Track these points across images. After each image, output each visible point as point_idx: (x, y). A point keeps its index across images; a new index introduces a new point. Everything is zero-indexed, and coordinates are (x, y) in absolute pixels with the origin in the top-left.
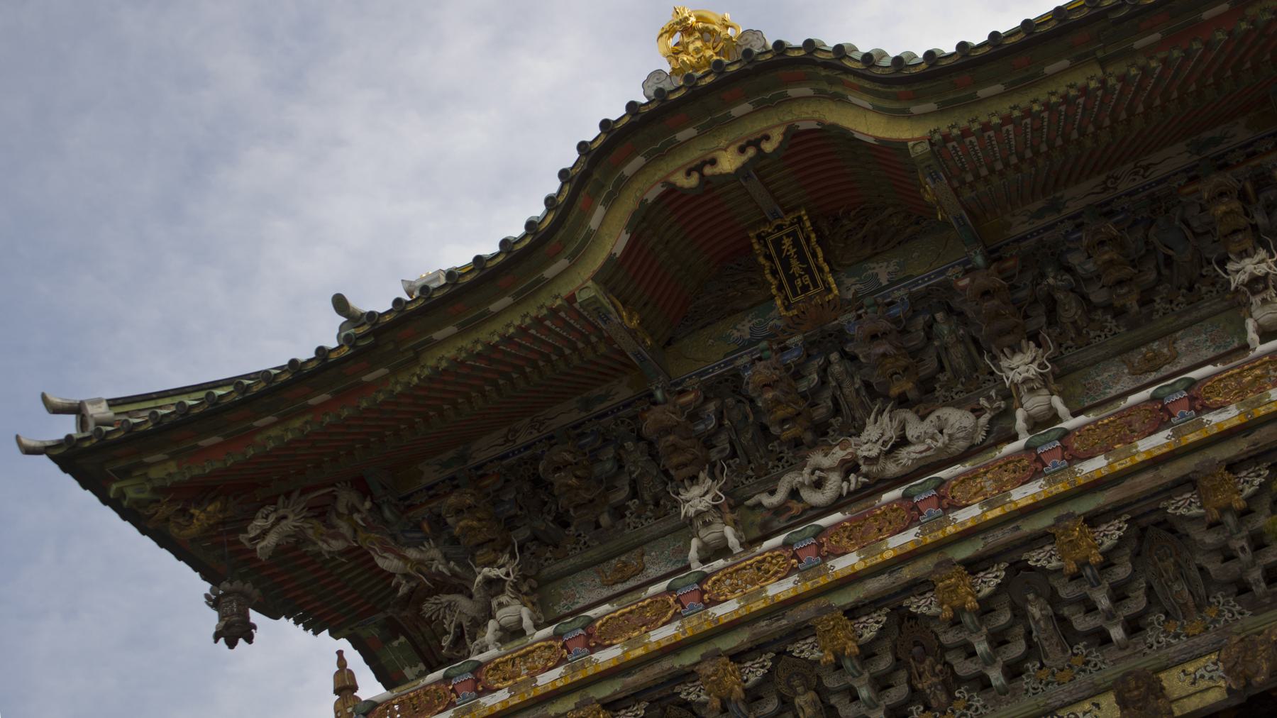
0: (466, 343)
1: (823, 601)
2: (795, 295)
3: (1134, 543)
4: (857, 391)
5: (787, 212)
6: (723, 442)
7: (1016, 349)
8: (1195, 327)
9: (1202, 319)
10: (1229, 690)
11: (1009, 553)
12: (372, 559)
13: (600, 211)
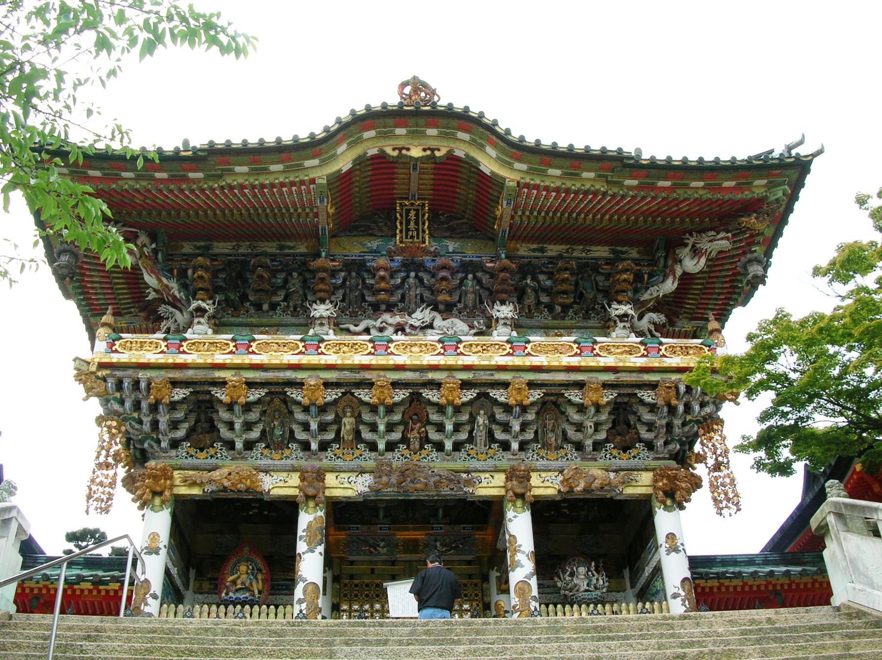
2: (407, 238)
3: (540, 406)
4: (416, 295)
5: (419, 199)
8: (583, 330)
9: (586, 328)
10: (559, 491)
12: (142, 274)
13: (344, 147)
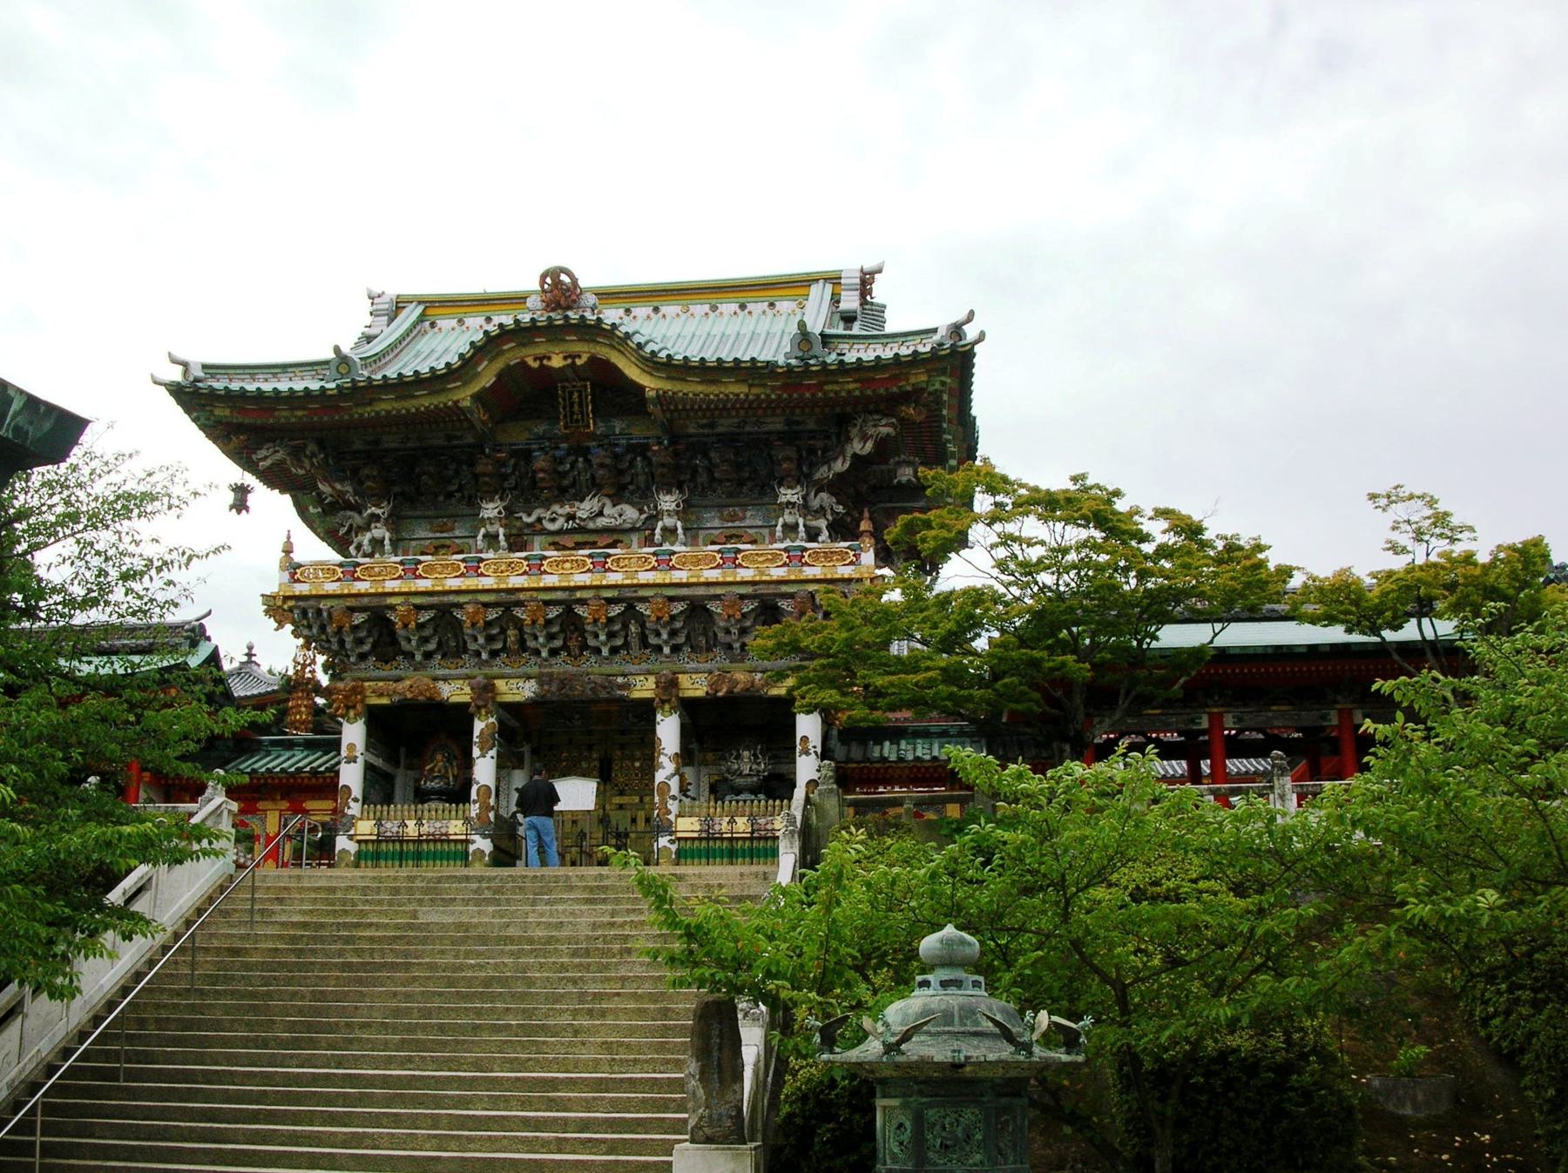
0: (395, 405)
1: (535, 594)
6: (512, 481)
7: (669, 492)
11: (628, 600)
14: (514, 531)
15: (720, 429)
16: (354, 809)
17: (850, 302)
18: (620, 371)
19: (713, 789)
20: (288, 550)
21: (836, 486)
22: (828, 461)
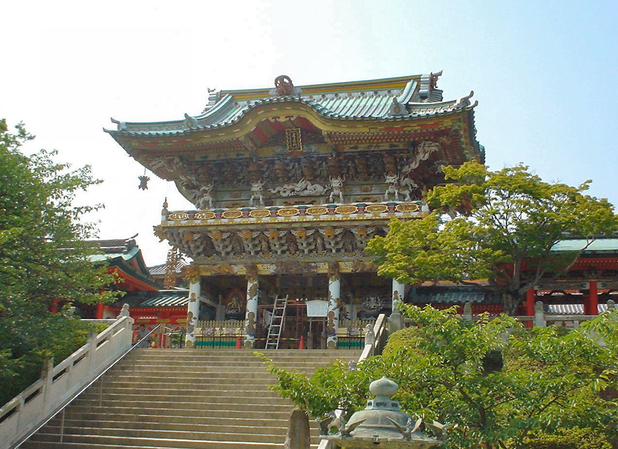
6: (267, 173)
7: (337, 178)
11: (315, 228)
14: (268, 197)
15: (359, 150)
16: (194, 322)
17: (424, 90)
18: (310, 122)
19: (359, 315)
20: (165, 205)
21: (413, 175)
22: (409, 164)
